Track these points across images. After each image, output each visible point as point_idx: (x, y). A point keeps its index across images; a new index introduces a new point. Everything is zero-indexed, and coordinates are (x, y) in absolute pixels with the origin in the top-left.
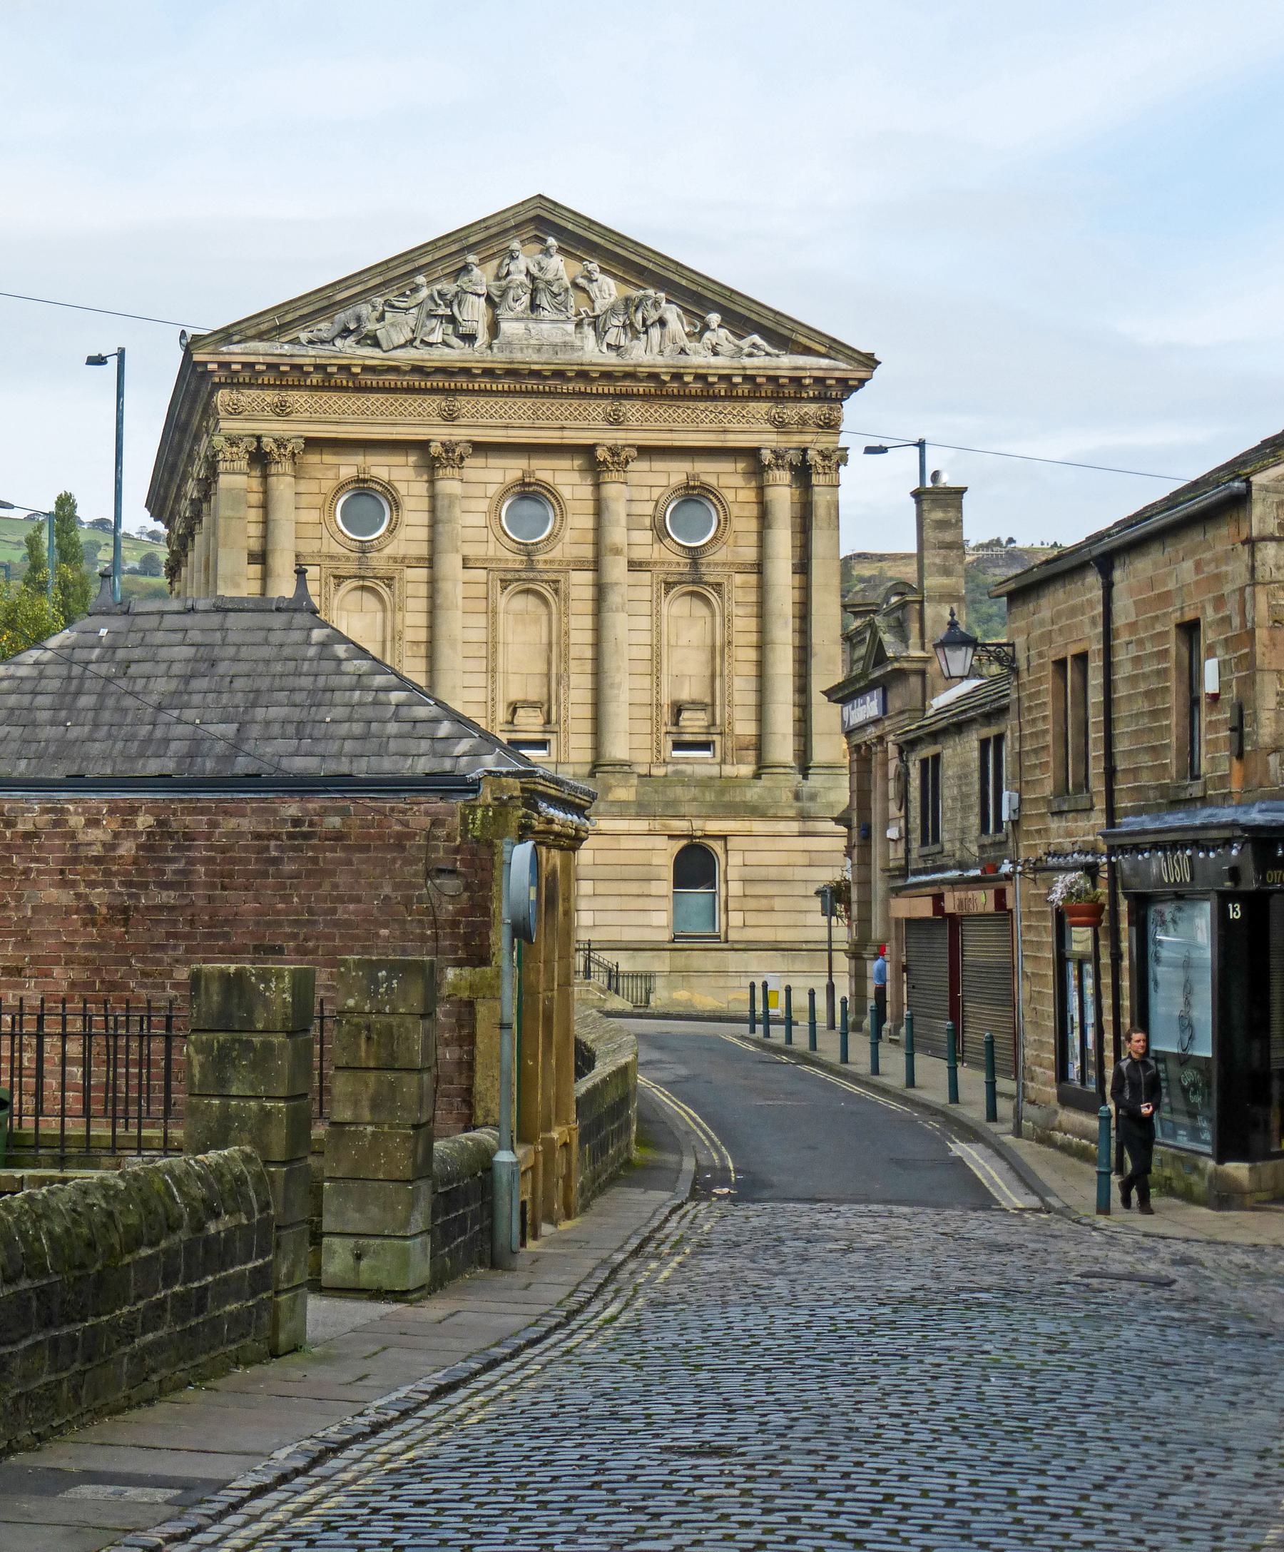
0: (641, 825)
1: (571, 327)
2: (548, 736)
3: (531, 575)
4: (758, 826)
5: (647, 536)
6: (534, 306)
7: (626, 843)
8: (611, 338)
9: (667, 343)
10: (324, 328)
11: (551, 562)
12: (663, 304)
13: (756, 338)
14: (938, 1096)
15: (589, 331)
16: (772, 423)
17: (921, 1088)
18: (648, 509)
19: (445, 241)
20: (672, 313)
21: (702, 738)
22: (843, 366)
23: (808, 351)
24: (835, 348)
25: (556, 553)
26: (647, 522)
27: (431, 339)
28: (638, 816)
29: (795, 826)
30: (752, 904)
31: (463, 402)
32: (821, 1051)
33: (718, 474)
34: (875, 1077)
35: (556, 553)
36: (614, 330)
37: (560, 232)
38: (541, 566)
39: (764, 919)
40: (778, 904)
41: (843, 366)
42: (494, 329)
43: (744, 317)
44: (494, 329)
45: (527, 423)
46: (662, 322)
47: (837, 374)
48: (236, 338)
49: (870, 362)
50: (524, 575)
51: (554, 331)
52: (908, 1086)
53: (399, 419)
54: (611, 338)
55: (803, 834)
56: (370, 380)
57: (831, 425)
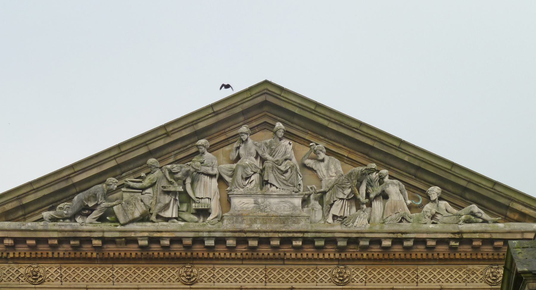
1: (298, 201)
6: (264, 183)
8: (335, 210)
9: (391, 210)
12: (386, 179)
13: (475, 208)
15: (314, 203)
16: (487, 282)
19: (176, 126)
20: (394, 189)
23: (524, 217)
27: (167, 214)
36: (339, 203)
37: (288, 116)
42: (226, 202)
44: (226, 202)
46: (385, 196)
51: (282, 205)
54: (335, 210)
56: (111, 250)
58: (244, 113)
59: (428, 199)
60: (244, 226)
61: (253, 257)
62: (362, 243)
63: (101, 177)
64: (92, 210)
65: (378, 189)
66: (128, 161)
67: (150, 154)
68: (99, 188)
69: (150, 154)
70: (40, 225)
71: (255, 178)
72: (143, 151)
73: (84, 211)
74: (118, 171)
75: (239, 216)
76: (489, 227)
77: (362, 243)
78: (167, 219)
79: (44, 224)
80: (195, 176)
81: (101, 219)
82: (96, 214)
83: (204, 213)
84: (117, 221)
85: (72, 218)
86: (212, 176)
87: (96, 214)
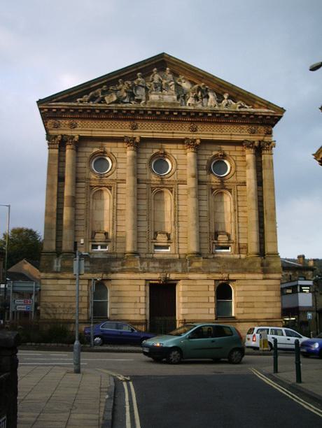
0: (204, 276)
1: (175, 97)
2: (229, 244)
3: (162, 186)
4: (248, 276)
5: (204, 172)
7: (199, 283)
10: (86, 97)
11: (170, 181)
14: (291, 377)
17: (303, 383)
18: (205, 163)
21: (226, 244)
22: (273, 112)
24: (268, 105)
25: (171, 178)
26: (205, 167)
27: (126, 101)
28: (203, 273)
29: (261, 276)
30: (246, 305)
31: (140, 124)
32: (303, 383)
33: (230, 151)
34: (300, 385)
35: (171, 178)
38: (166, 183)
39: (251, 310)
40: (256, 305)
41: (273, 112)
43: (237, 94)
44: (147, 98)
45: (161, 131)
47: (271, 114)
48: (55, 100)
49: (283, 111)
50: (160, 186)
52: (297, 381)
53: (114, 130)
55: (264, 279)
57: (269, 133)
58: (155, 64)
59: (224, 99)
60: (155, 106)
61: (261, 171)
62: (192, 114)
63: (100, 86)
64: (97, 98)
65: (206, 94)
66: (110, 81)
67: (120, 78)
68: (99, 90)
69: (120, 78)
70: (75, 104)
71: (159, 88)
72: (117, 77)
73: (93, 99)
74: (316, 302)
75: (153, 103)
76: (249, 110)
77: (200, 114)
78: (125, 103)
79: (83, 102)
80: (136, 87)
81: (100, 102)
82: (98, 100)
83: (139, 101)
84: (106, 103)
85: (89, 102)
86: (143, 87)
87: (98, 100)
